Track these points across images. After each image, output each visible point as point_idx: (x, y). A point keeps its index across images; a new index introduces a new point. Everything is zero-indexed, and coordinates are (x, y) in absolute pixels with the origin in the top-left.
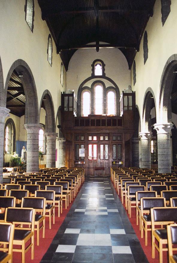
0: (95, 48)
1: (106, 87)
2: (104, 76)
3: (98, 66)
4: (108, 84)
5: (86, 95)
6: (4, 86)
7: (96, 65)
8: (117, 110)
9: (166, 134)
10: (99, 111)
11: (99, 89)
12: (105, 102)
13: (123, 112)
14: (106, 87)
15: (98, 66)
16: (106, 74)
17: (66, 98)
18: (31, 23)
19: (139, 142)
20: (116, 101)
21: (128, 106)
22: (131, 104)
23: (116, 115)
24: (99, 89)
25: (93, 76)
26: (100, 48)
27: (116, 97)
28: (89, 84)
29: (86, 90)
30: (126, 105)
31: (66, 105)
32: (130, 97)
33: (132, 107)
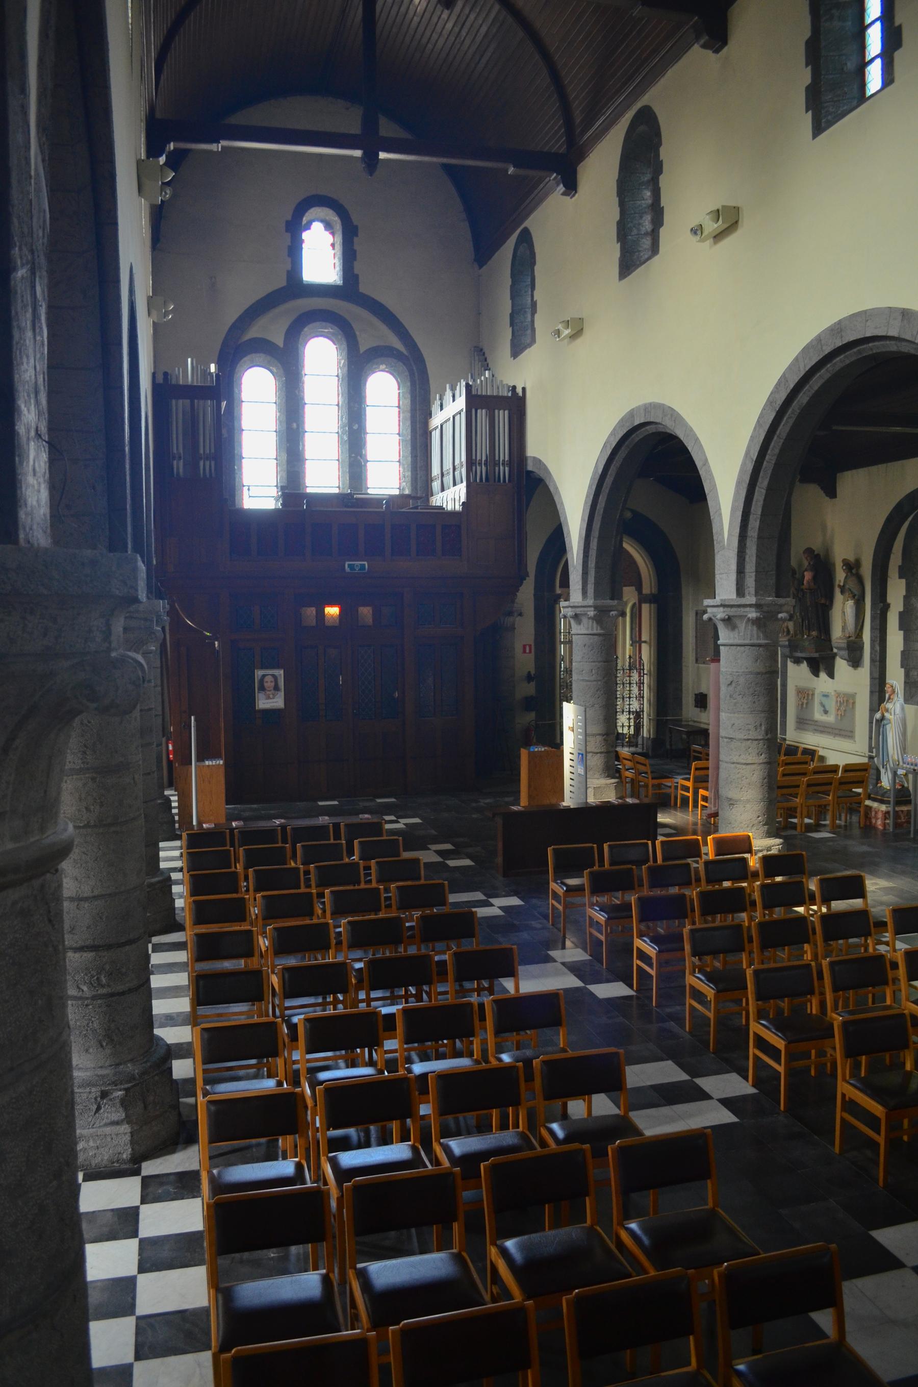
0: (358, 153)
1: (362, 349)
2: (350, 288)
3: (317, 226)
4: (375, 332)
5: (257, 386)
6: (807, 1345)
7: (308, 227)
8: (414, 468)
9: (760, 646)
10: (323, 477)
11: (321, 356)
12: (356, 427)
13: (468, 487)
14: (362, 349)
15: (317, 226)
16: (361, 278)
17: (179, 406)
18: (873, 56)
19: (514, 624)
20: (408, 423)
21: (492, 461)
22: (503, 453)
23: (407, 492)
24: (321, 356)
25: (295, 287)
26: (382, 155)
27: (408, 401)
28: (272, 329)
29: (256, 350)
30: (482, 453)
31: (177, 445)
32: (503, 417)
33: (510, 463)
